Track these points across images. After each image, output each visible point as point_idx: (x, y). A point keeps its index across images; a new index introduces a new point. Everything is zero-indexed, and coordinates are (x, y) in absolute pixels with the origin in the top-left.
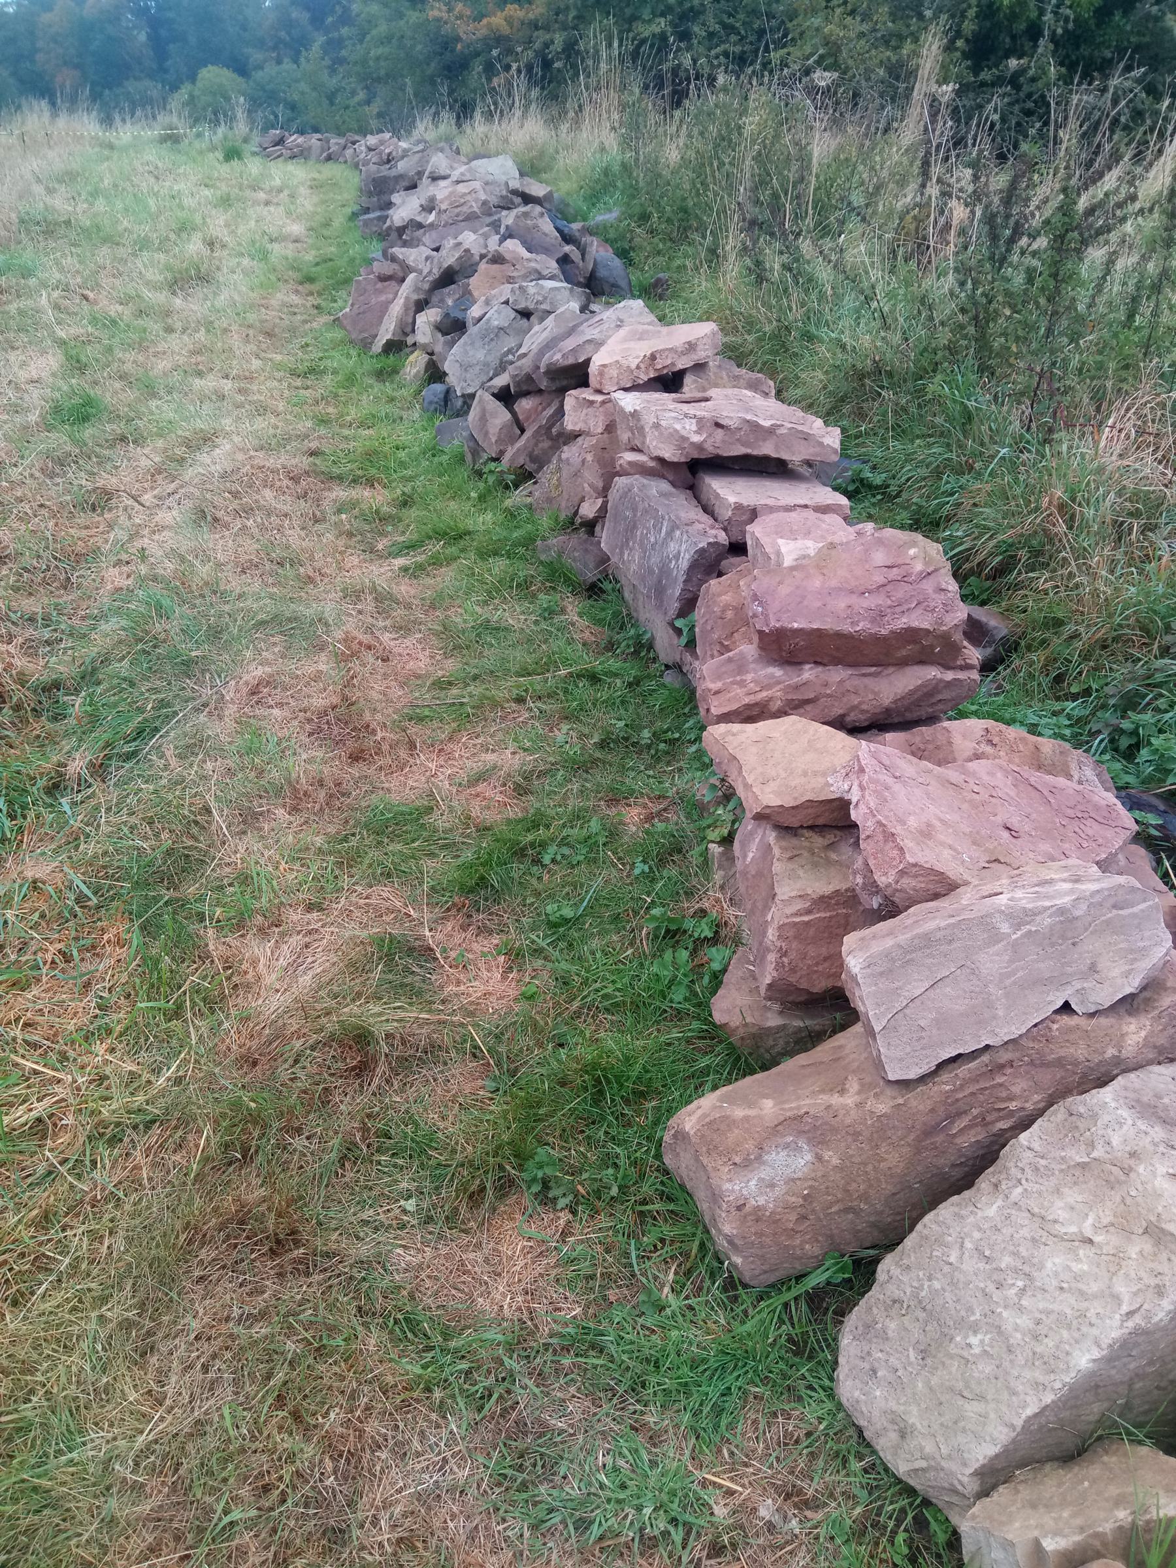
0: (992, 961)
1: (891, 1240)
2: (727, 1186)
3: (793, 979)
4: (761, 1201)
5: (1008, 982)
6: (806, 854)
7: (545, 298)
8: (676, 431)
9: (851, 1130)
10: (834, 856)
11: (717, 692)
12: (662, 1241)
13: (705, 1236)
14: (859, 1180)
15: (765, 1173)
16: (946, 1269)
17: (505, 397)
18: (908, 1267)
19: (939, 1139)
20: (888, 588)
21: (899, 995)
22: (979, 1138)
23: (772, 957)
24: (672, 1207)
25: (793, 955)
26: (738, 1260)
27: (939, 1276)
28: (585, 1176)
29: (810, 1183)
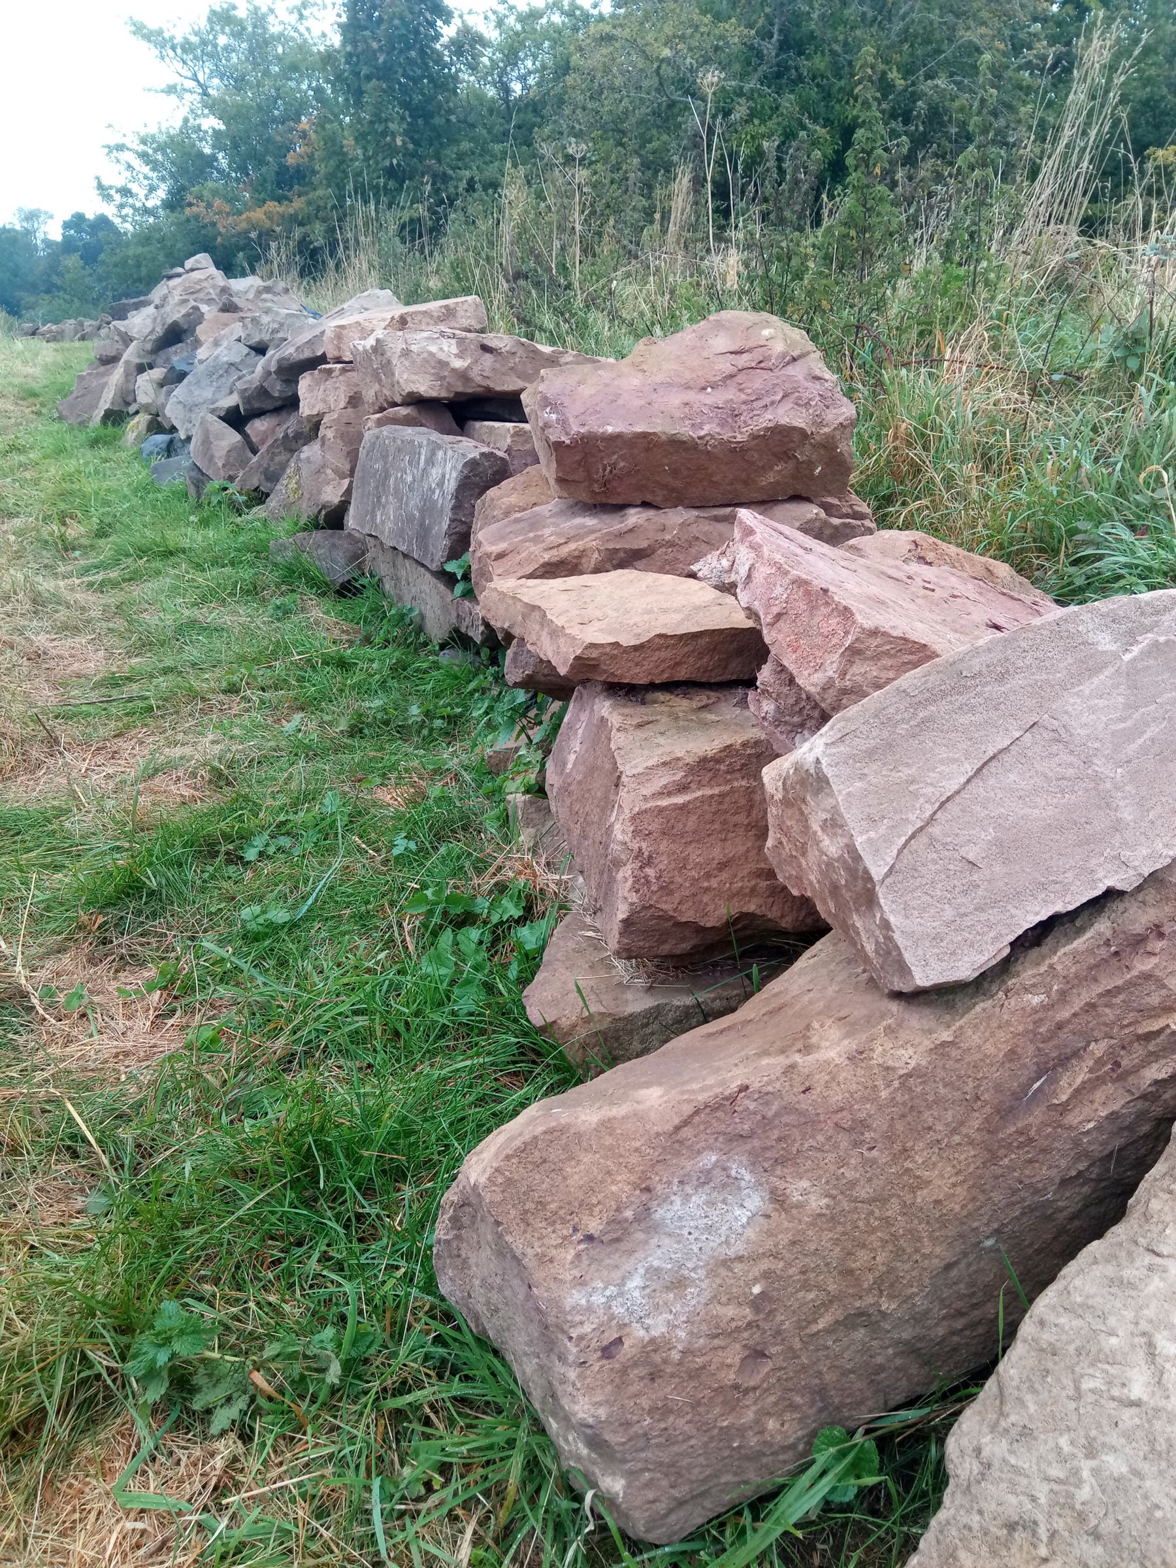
0: (1093, 710)
1: (969, 1367)
2: (575, 1298)
3: (667, 906)
4: (658, 1326)
5: (1132, 748)
6: (664, 719)
7: (282, 325)
8: (432, 354)
9: (845, 1119)
10: (712, 717)
11: (501, 556)
12: (445, 1469)
13: (535, 1440)
14: (874, 1240)
15: (659, 1254)
16: (1129, 1418)
17: (236, 419)
18: (1026, 1433)
19: (1036, 1117)
20: (740, 378)
21: (915, 795)
22: (1116, 1107)
23: (625, 873)
24: (457, 1388)
25: (663, 862)
26: (615, 1485)
27: (1114, 1438)
28: (271, 1350)
29: (765, 1264)
